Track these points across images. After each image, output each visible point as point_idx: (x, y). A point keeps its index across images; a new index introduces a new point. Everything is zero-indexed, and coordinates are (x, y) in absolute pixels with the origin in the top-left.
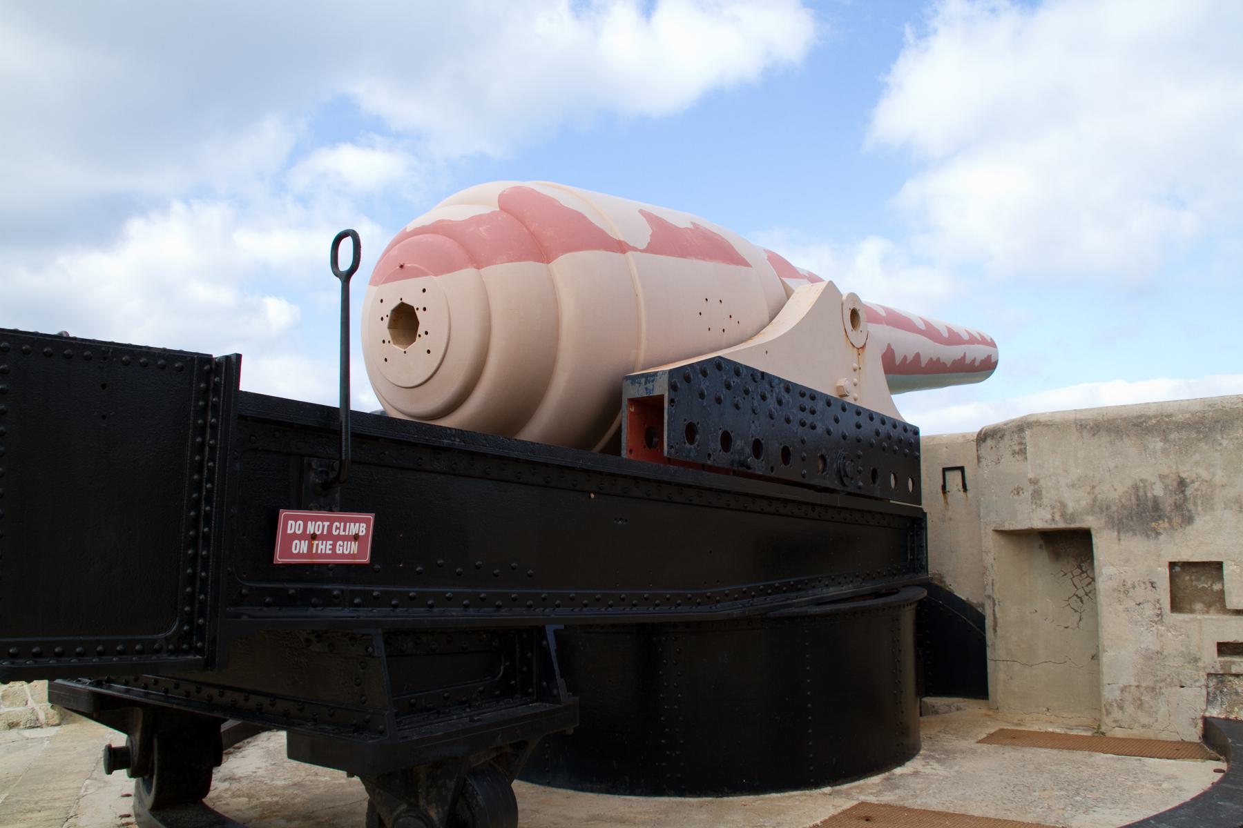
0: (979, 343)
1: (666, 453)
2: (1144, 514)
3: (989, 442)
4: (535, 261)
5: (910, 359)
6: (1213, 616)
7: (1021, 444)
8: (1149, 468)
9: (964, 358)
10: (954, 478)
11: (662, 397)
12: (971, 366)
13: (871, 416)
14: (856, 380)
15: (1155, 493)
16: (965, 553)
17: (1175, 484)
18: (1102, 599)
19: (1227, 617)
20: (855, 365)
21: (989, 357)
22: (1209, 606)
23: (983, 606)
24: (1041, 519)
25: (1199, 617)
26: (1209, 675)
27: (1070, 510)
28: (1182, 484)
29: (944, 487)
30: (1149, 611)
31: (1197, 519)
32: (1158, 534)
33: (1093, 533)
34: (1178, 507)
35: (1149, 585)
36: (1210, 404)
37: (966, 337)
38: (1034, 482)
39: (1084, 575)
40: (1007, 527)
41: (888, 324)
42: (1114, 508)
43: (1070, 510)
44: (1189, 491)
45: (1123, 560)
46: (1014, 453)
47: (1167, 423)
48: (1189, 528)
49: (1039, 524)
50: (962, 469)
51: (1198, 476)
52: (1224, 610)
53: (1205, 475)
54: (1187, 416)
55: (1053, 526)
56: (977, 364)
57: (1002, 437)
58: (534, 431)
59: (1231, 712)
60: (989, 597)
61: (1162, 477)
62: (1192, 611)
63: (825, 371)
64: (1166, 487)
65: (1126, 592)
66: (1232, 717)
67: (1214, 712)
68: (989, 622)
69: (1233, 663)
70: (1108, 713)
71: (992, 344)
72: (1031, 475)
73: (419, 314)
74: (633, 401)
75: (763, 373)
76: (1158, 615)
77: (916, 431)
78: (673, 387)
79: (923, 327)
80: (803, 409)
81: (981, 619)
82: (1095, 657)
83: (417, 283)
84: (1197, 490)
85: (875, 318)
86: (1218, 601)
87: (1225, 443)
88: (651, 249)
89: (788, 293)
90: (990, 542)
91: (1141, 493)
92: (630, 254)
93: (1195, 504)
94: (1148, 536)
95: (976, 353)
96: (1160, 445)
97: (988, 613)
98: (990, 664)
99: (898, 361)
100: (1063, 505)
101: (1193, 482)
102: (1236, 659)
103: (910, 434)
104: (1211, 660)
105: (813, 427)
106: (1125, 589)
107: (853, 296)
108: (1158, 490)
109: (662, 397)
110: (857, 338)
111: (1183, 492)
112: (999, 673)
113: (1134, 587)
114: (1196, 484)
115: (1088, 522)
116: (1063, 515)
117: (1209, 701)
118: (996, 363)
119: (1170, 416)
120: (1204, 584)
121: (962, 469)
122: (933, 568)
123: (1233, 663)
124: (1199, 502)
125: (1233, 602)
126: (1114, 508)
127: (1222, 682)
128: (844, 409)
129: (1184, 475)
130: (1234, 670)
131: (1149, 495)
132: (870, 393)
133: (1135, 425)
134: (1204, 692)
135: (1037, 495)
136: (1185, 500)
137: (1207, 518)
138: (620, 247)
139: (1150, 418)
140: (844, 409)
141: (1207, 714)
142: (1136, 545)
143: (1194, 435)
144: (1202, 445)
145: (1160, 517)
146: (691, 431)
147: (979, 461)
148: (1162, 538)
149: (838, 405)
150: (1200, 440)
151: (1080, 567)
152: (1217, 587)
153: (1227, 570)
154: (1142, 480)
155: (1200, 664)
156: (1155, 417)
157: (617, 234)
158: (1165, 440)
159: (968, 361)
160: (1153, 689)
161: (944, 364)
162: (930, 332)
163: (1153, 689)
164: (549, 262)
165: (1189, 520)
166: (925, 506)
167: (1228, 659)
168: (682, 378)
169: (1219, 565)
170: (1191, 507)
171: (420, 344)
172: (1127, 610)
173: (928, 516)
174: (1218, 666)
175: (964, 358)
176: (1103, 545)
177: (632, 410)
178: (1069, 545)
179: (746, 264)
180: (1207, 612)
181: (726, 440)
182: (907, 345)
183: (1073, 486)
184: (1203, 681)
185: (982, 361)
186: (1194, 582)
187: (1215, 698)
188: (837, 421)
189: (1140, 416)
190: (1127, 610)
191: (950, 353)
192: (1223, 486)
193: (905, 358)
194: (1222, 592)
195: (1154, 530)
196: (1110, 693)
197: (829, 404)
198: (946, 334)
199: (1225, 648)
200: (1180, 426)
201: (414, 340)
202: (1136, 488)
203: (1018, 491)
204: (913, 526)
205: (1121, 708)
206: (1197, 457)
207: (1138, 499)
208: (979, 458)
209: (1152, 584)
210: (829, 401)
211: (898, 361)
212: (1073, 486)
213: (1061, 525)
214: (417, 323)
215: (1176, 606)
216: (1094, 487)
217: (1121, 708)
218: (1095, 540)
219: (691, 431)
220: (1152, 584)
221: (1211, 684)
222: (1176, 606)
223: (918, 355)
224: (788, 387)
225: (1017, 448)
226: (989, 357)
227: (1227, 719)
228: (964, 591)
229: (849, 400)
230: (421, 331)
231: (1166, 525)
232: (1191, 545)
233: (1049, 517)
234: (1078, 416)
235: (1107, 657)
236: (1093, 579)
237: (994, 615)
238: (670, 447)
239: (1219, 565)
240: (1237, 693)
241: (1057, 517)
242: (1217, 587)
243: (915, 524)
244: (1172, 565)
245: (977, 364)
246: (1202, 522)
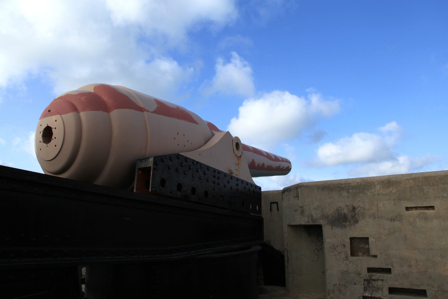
0: (285, 161)
1: (150, 190)
2: (341, 220)
3: (286, 193)
4: (103, 111)
5: (260, 165)
6: (365, 258)
7: (297, 193)
8: (342, 203)
9: (280, 166)
10: (275, 206)
11: (151, 167)
12: (281, 168)
13: (243, 182)
14: (237, 168)
15: (345, 212)
16: (277, 233)
17: (351, 208)
18: (326, 251)
19: (370, 258)
20: (237, 163)
21: (288, 167)
22: (364, 254)
23: (284, 252)
24: (304, 221)
25: (361, 258)
26: (365, 280)
27: (314, 218)
28: (354, 208)
29: (271, 209)
30: (343, 256)
31: (359, 221)
32: (346, 227)
33: (323, 226)
34: (353, 217)
35: (343, 246)
36: (363, 179)
37: (281, 159)
38: (301, 207)
39: (319, 242)
40: (292, 224)
41: (253, 152)
42: (330, 217)
43: (314, 218)
44: (357, 211)
45: (333, 236)
46: (294, 197)
47: (349, 186)
48: (357, 225)
49: (303, 223)
50: (277, 203)
51: (360, 206)
52: (369, 255)
53: (362, 205)
54: (355, 184)
55: (308, 224)
56: (284, 168)
57: (290, 191)
58: (101, 181)
59: (373, 294)
60: (286, 249)
61: (347, 206)
62: (358, 256)
63: (223, 163)
64: (348, 210)
65: (335, 249)
66: (373, 296)
67: (367, 294)
68: (286, 258)
69: (373, 275)
70: (329, 294)
71: (290, 162)
72: (300, 205)
73: (53, 130)
74: (140, 169)
75: (198, 162)
76: (346, 257)
77: (260, 188)
78: (155, 163)
79: (266, 155)
80: (214, 177)
81: (283, 257)
82: (324, 272)
83: (54, 118)
84: (359, 211)
85: (246, 148)
86: (367, 252)
87: (369, 194)
88: (155, 112)
89: (213, 135)
90: (286, 229)
91: (339, 212)
92: (145, 112)
93: (359, 216)
94: (342, 228)
95: (285, 165)
96: (346, 194)
97: (286, 254)
98: (286, 274)
99: (256, 165)
100: (312, 216)
101: (358, 208)
102: (374, 274)
103: (258, 189)
104: (365, 273)
105: (218, 184)
106: (334, 248)
107: (237, 138)
108: (346, 211)
109: (151, 167)
110: (238, 153)
111: (354, 211)
112: (289, 278)
113: (337, 247)
114: (359, 209)
115: (321, 222)
116: (312, 220)
117: (365, 290)
118: (291, 169)
119: (349, 184)
120: (362, 245)
121: (277, 203)
122: (266, 239)
123: (373, 275)
124: (360, 215)
125: (373, 252)
126: (330, 217)
127: (369, 282)
128: (232, 179)
129: (355, 205)
130: (373, 278)
131: (342, 212)
132: (242, 173)
133: (337, 187)
134: (363, 286)
135: (303, 212)
136: (355, 214)
137: (363, 221)
138: (141, 110)
139: (343, 184)
140: (232, 179)
141: (364, 295)
142: (338, 231)
143: (358, 191)
144: (361, 194)
145: (346, 221)
146: (163, 182)
147: (283, 200)
148: (347, 228)
149: (230, 177)
150: (360, 193)
151: (318, 239)
152: (366, 247)
153: (371, 240)
154: (340, 207)
155: (361, 276)
156: (344, 184)
157: (142, 105)
158: (348, 193)
159: (281, 167)
160: (345, 285)
161: (273, 168)
162: (268, 156)
163: (345, 285)
164: (109, 112)
165: (357, 222)
166: (264, 215)
167: (371, 274)
168: (160, 160)
169: (367, 238)
170: (357, 217)
171: (53, 142)
172: (335, 255)
173: (264, 220)
174: (368, 277)
175: (280, 166)
176: (327, 231)
177: (140, 173)
178: (314, 231)
179: (197, 123)
180: (363, 256)
181: (179, 187)
182: (259, 160)
183: (315, 209)
184: (362, 282)
185: (286, 168)
186: (359, 245)
187: (367, 289)
188: (228, 182)
189: (339, 184)
190: (335, 255)
191: (275, 164)
192: (368, 210)
193: (259, 164)
194: (368, 249)
195: (344, 225)
196: (329, 287)
197: (225, 176)
198: (274, 158)
199: (370, 270)
200: (354, 187)
201: (50, 141)
202: (338, 210)
203: (296, 211)
204: (259, 222)
205: (333, 292)
206: (359, 199)
207: (338, 214)
208: (282, 199)
209: (344, 245)
210: (225, 175)
211: (256, 165)
212: (315, 209)
213: (311, 223)
214: (52, 134)
215: (353, 254)
216: (323, 210)
217: (333, 292)
218: (323, 229)
219: (163, 182)
220: (344, 245)
221: (365, 283)
222: (353, 254)
223: (263, 164)
224: (208, 168)
225: (295, 195)
226: (288, 167)
227: (371, 297)
228: (277, 247)
229: (234, 175)
230: (53, 137)
231: (349, 224)
232: (357, 231)
233: (307, 220)
234: (317, 184)
235: (328, 273)
236: (323, 243)
237: (288, 256)
238: (152, 188)
239: (367, 238)
240: (374, 287)
241: (310, 220)
242: (366, 247)
243: (260, 222)
244: (352, 239)
245: (284, 168)
246: (362, 223)
